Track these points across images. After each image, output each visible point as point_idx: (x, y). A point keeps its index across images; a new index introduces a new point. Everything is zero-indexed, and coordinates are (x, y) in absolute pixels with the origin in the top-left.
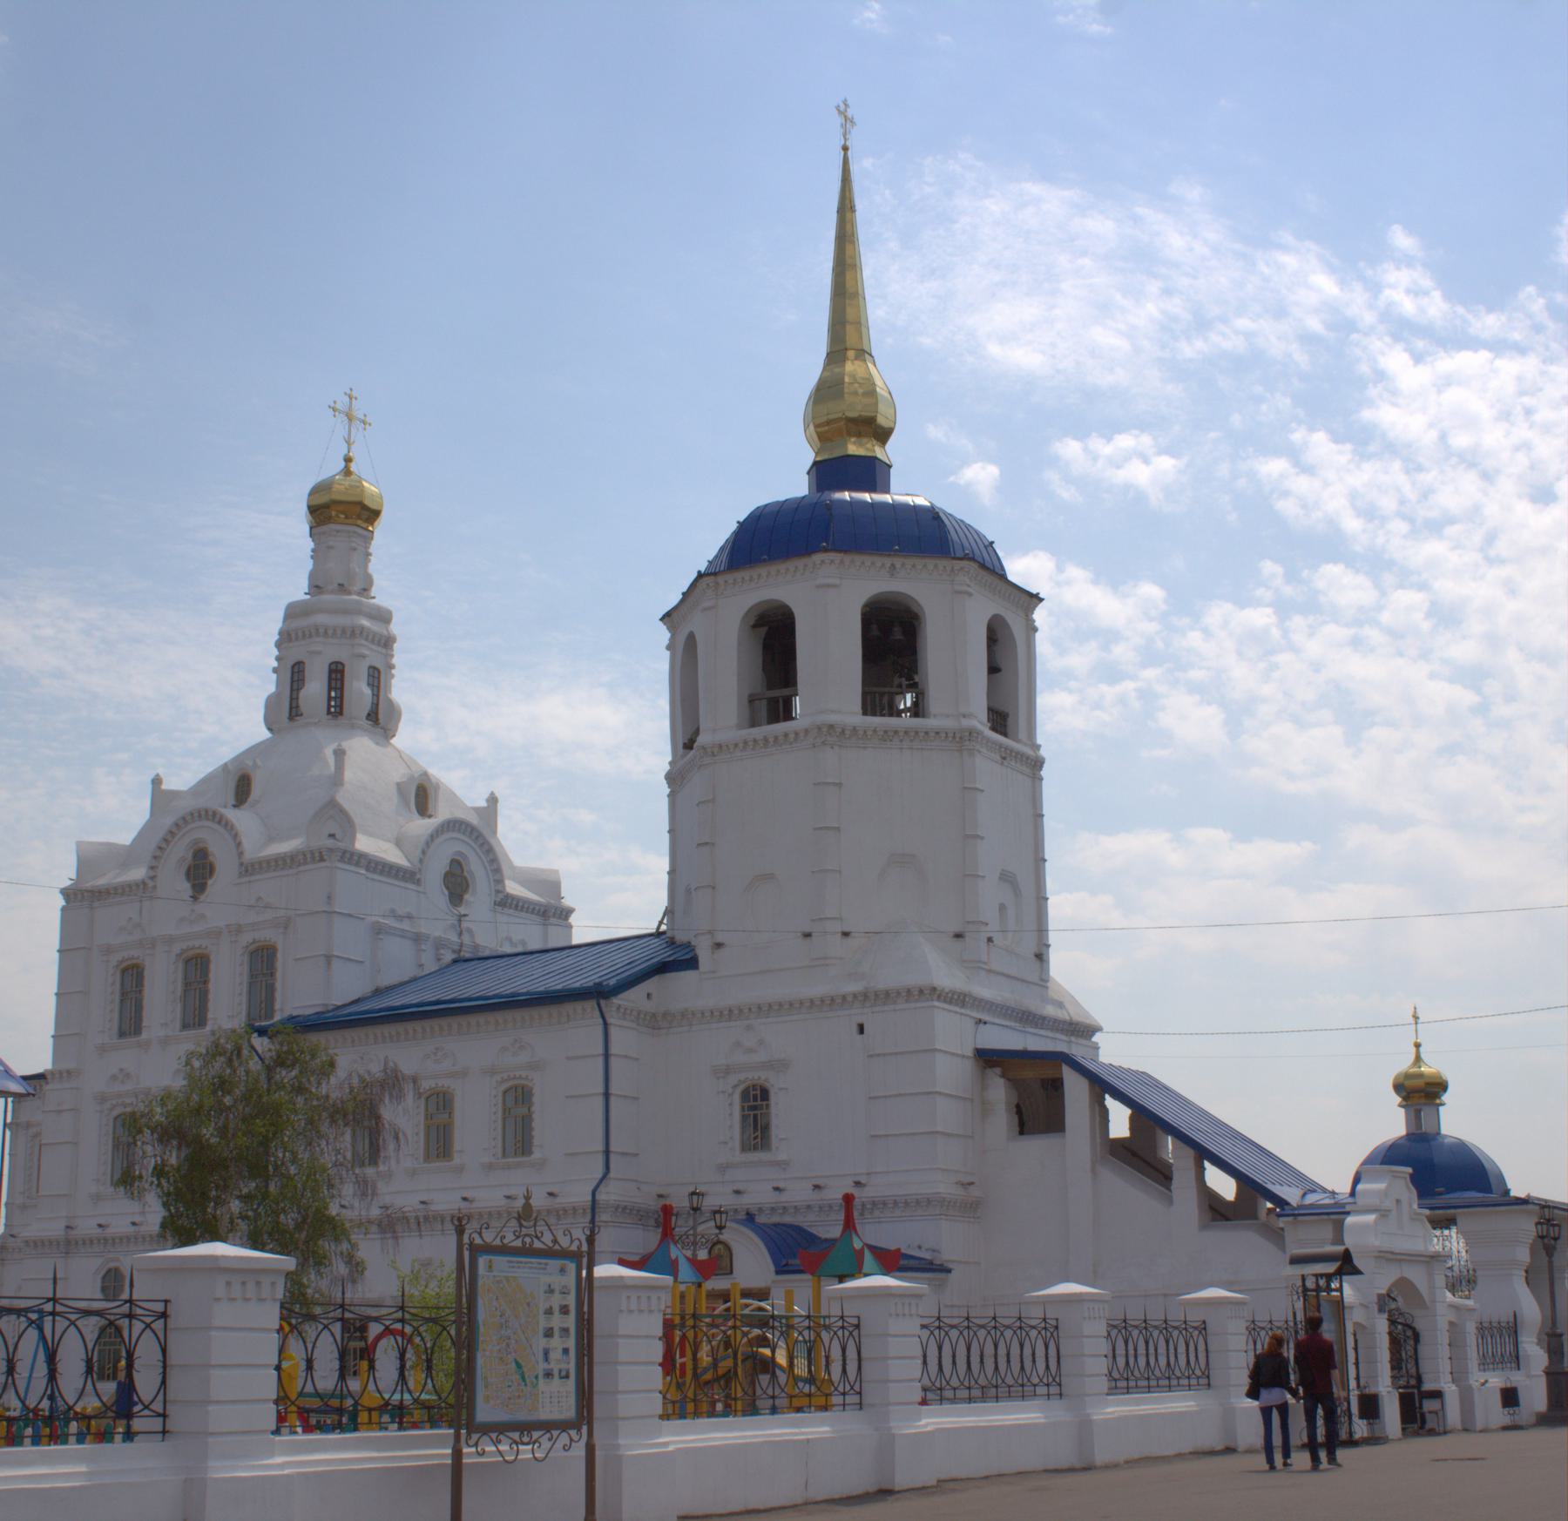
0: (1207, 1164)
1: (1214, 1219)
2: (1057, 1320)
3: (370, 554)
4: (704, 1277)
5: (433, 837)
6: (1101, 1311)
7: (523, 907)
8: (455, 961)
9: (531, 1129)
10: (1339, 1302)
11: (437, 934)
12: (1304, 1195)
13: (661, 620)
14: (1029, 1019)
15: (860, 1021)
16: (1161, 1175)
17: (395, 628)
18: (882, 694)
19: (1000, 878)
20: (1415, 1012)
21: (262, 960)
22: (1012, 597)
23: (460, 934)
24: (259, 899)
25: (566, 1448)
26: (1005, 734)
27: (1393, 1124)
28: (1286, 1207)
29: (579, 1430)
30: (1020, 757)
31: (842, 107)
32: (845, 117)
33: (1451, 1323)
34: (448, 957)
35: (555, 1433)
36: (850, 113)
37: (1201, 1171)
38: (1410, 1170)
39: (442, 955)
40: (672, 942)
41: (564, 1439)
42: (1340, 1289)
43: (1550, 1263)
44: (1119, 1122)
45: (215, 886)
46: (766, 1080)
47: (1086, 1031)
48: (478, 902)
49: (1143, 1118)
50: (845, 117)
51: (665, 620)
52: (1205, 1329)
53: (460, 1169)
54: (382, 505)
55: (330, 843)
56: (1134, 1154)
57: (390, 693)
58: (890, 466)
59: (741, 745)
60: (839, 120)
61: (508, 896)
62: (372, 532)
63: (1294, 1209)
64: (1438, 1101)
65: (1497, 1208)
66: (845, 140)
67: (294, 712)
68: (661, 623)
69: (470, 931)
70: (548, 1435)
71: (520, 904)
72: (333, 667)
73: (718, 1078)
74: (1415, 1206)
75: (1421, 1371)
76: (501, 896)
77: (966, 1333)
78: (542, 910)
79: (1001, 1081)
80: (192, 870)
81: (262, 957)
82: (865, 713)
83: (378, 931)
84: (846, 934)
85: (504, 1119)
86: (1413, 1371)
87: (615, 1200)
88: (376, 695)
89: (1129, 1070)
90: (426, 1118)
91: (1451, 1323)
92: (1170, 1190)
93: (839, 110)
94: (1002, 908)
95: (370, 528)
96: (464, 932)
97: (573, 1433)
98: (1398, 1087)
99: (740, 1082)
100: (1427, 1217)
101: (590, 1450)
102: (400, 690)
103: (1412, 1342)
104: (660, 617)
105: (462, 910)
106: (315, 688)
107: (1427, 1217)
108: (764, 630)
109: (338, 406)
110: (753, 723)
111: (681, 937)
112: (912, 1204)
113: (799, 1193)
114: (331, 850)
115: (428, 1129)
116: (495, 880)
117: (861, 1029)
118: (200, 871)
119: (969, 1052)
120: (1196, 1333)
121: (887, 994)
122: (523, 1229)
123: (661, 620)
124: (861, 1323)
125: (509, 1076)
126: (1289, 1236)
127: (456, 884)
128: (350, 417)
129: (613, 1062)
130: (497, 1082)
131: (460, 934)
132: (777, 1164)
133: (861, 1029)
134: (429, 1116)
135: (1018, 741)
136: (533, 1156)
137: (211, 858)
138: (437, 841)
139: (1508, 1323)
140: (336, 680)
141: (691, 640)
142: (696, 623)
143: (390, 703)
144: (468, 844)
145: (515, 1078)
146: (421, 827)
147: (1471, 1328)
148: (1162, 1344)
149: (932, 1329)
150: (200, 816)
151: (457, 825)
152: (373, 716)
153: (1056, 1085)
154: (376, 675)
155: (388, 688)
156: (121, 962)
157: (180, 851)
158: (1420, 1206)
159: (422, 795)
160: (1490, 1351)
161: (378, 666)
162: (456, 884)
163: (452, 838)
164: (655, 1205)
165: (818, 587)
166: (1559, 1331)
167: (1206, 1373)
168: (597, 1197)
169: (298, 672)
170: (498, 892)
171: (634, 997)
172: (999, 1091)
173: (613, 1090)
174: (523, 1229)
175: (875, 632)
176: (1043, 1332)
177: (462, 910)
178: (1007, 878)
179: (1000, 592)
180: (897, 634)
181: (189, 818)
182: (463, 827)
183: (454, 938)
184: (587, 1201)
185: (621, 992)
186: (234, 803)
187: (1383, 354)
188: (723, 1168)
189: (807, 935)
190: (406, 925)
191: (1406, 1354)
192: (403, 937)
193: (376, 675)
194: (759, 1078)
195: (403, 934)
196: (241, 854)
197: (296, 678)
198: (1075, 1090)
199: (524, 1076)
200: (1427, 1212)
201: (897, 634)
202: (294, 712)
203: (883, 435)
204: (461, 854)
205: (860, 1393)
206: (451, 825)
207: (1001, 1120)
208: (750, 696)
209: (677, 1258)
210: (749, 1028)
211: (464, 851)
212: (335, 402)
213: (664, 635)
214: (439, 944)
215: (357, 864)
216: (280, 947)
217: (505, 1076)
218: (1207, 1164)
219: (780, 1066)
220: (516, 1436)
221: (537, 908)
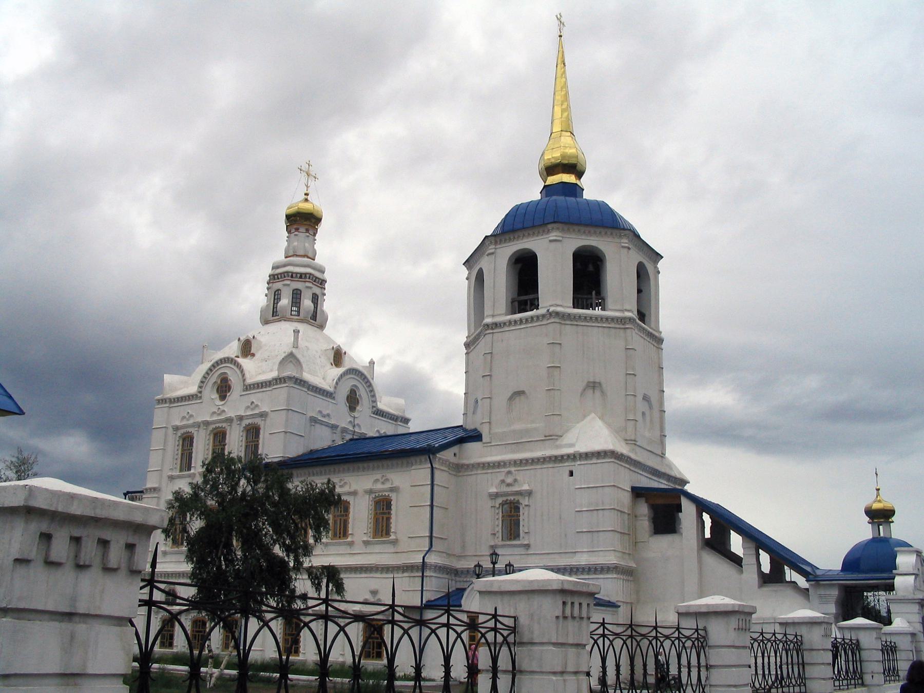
0: (761, 551)
2: (515, 618)
3: (315, 240)
5: (342, 376)
7: (385, 416)
11: (343, 425)
13: (463, 264)
14: (656, 473)
15: (571, 469)
17: (326, 276)
18: (582, 298)
19: (643, 399)
20: (876, 471)
21: (253, 432)
24: (253, 403)
26: (644, 322)
27: (864, 532)
30: (651, 335)
31: (559, 16)
32: (560, 22)
36: (562, 20)
39: (345, 436)
40: (465, 430)
47: (684, 482)
48: (364, 408)
50: (560, 22)
51: (465, 264)
53: (351, 544)
54: (322, 216)
57: (323, 307)
58: (583, 190)
59: (507, 324)
60: (557, 22)
61: (378, 410)
62: (317, 229)
64: (890, 520)
65: (837, 579)
66: (560, 32)
68: (464, 266)
71: (384, 414)
72: (295, 292)
76: (374, 409)
77: (629, 642)
80: (220, 388)
81: (253, 432)
82: (574, 308)
83: (314, 420)
87: (435, 563)
88: (316, 308)
92: (742, 567)
93: (557, 18)
94: (643, 414)
95: (316, 227)
102: (328, 305)
104: (463, 263)
108: (519, 266)
109: (303, 168)
110: (514, 313)
112: (586, 570)
116: (372, 401)
117: (571, 474)
120: (769, 644)
123: (463, 264)
125: (379, 495)
127: (353, 401)
128: (308, 175)
129: (436, 488)
130: (372, 497)
133: (571, 474)
137: (229, 382)
138: (341, 381)
140: (296, 298)
142: (485, 263)
143: (323, 311)
144: (359, 381)
146: (337, 372)
148: (773, 654)
149: (624, 638)
150: (225, 361)
151: (351, 371)
152: (314, 317)
154: (316, 298)
155: (322, 305)
157: (214, 378)
159: (338, 356)
161: (317, 293)
162: (353, 401)
163: (351, 378)
165: (551, 241)
166: (582, 616)
168: (425, 560)
169: (277, 299)
170: (373, 407)
171: (447, 455)
172: (644, 509)
173: (435, 504)
176: (676, 642)
178: (646, 398)
179: (642, 250)
180: (591, 268)
181: (215, 365)
184: (420, 563)
185: (441, 451)
187: (920, 632)
188: (171, 478)
192: (327, 426)
193: (316, 298)
194: (514, 499)
196: (244, 380)
197: (276, 298)
198: (688, 510)
199: (387, 495)
201: (591, 268)
203: (580, 174)
204: (355, 386)
207: (645, 524)
208: (512, 299)
210: (509, 473)
211: (357, 385)
212: (301, 166)
213: (465, 272)
214: (344, 430)
215: (303, 386)
216: (262, 427)
218: (761, 551)
221: (393, 417)
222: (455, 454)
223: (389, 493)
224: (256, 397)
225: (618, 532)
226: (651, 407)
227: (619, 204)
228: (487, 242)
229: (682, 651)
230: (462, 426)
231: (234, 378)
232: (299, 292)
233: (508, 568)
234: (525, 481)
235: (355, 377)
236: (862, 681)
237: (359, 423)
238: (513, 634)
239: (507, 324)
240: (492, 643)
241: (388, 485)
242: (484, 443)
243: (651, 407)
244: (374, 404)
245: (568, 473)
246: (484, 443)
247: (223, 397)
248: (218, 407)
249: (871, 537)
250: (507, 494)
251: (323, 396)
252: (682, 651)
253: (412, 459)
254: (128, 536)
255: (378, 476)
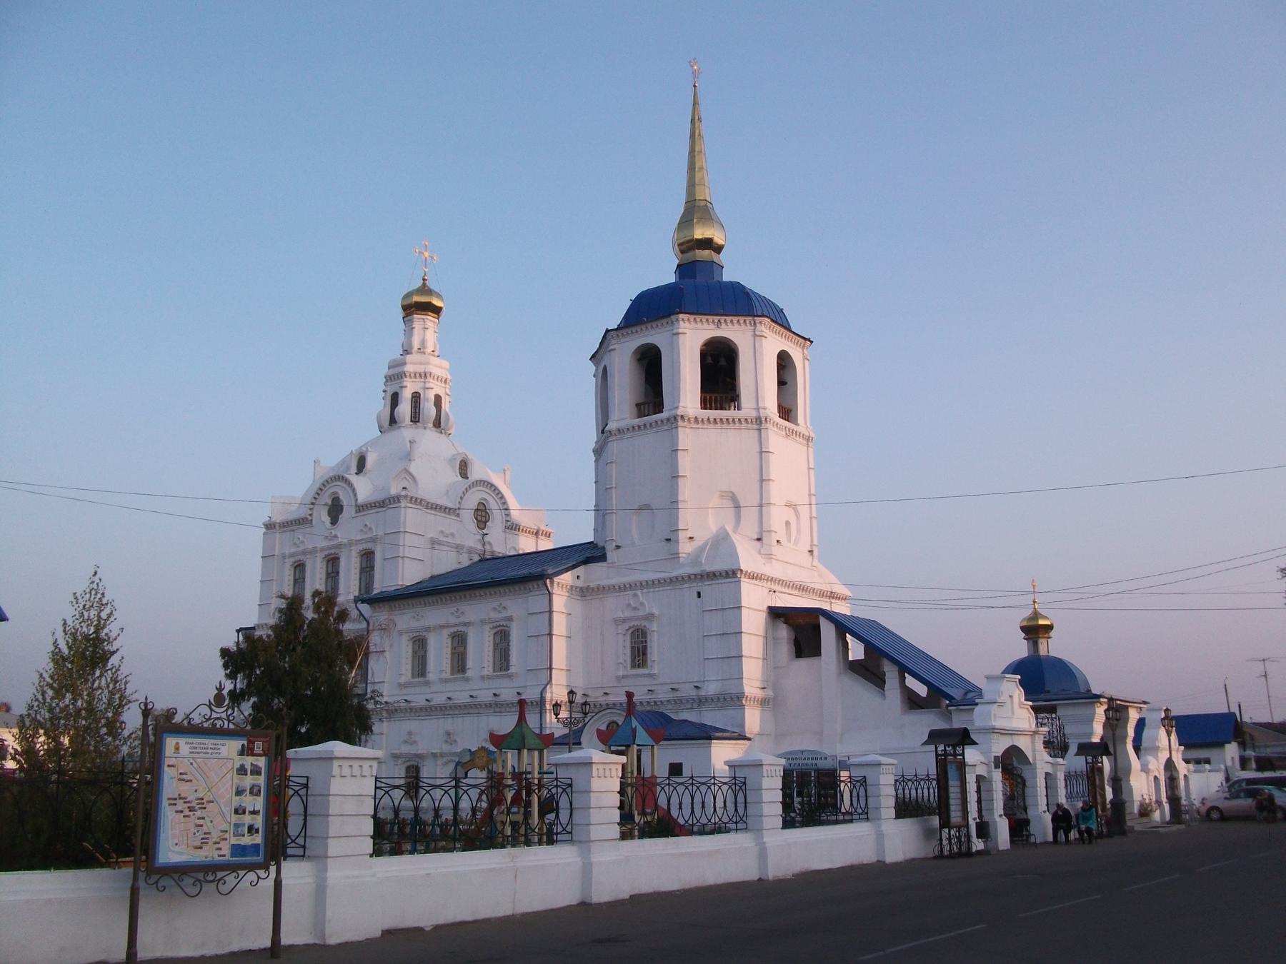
1: (911, 708)
2: (745, 778)
4: (655, 741)
6: (769, 772)
8: (480, 561)
9: (509, 656)
10: (961, 762)
11: (470, 545)
12: (966, 694)
13: (590, 359)
16: (878, 680)
22: (793, 340)
23: (484, 544)
25: (253, 884)
27: (1020, 649)
28: (953, 701)
29: (267, 869)
33: (1047, 774)
34: (476, 558)
35: (242, 873)
37: (903, 679)
38: (1019, 677)
41: (251, 876)
42: (963, 754)
43: (1114, 735)
44: (856, 651)
45: (343, 518)
46: (645, 626)
49: (870, 648)
52: (865, 781)
55: (403, 493)
56: (867, 669)
63: (958, 701)
67: (393, 421)
69: (490, 543)
70: (235, 874)
71: (755, 575)
73: (618, 625)
74: (1023, 699)
75: (1027, 804)
77: (667, 788)
78: (535, 531)
79: (784, 626)
84: (691, 538)
85: (494, 652)
86: (1021, 804)
89: (863, 619)
90: (452, 649)
91: (1047, 774)
94: (788, 523)
96: (486, 544)
97: (262, 873)
98: (1023, 629)
99: (630, 628)
100: (1031, 706)
101: (278, 884)
103: (1021, 786)
105: (485, 531)
106: (405, 409)
107: (1031, 706)
111: (601, 544)
113: (662, 694)
114: (405, 497)
115: (453, 654)
117: (699, 595)
118: (335, 510)
119: (765, 608)
121: (714, 574)
122: (213, 713)
124: (573, 783)
126: (954, 716)
127: (482, 515)
131: (484, 544)
132: (651, 676)
133: (699, 595)
134: (454, 648)
135: (797, 425)
136: (509, 671)
138: (470, 492)
139: (1082, 772)
141: (605, 369)
145: (499, 626)
147: (1061, 776)
152: (437, 424)
153: (816, 629)
156: (295, 563)
157: (326, 499)
158: (1026, 700)
160: (1081, 790)
162: (482, 515)
164: (516, 699)
167: (866, 811)
172: (784, 632)
174: (213, 713)
175: (709, 360)
177: (485, 531)
180: (723, 362)
181: (329, 480)
182: (486, 484)
183: (480, 547)
186: (356, 471)
188: (619, 678)
189: (668, 540)
190: (449, 540)
191: (1017, 793)
195: (448, 544)
196: (357, 500)
198: (828, 632)
200: (1031, 703)
201: (723, 362)
202: (393, 421)
205: (571, 833)
206: (478, 482)
207: (785, 649)
209: (636, 727)
213: (592, 368)
214: (470, 551)
217: (495, 624)
219: (650, 617)
220: (200, 876)
222: (578, 577)
223: (507, 623)
224: (370, 518)
225: (754, 658)
226: (797, 515)
227: (753, 283)
228: (609, 337)
229: (647, 793)
230: (592, 542)
231: (345, 499)
232: (418, 395)
233: (555, 707)
234: (651, 603)
235: (484, 489)
236: (1215, 820)
237: (491, 541)
238: (305, 789)
239: (631, 429)
240: (304, 795)
241: (504, 614)
242: (609, 563)
243: (797, 515)
244: (508, 519)
245: (696, 595)
246: (609, 563)
247: (334, 521)
248: (330, 531)
249: (1027, 655)
250: (631, 619)
251: (445, 513)
252: (647, 793)
253: (530, 585)
254: (382, 638)
255: (496, 604)
